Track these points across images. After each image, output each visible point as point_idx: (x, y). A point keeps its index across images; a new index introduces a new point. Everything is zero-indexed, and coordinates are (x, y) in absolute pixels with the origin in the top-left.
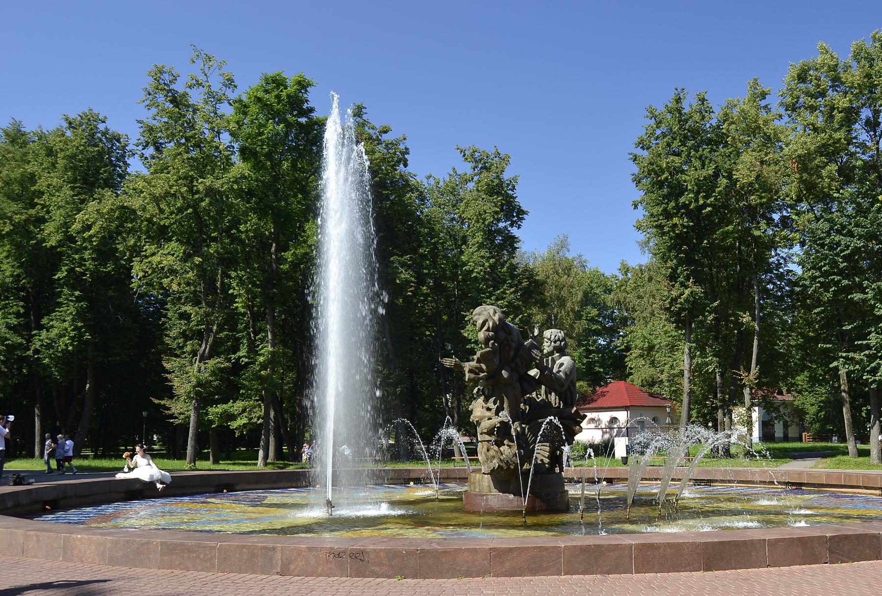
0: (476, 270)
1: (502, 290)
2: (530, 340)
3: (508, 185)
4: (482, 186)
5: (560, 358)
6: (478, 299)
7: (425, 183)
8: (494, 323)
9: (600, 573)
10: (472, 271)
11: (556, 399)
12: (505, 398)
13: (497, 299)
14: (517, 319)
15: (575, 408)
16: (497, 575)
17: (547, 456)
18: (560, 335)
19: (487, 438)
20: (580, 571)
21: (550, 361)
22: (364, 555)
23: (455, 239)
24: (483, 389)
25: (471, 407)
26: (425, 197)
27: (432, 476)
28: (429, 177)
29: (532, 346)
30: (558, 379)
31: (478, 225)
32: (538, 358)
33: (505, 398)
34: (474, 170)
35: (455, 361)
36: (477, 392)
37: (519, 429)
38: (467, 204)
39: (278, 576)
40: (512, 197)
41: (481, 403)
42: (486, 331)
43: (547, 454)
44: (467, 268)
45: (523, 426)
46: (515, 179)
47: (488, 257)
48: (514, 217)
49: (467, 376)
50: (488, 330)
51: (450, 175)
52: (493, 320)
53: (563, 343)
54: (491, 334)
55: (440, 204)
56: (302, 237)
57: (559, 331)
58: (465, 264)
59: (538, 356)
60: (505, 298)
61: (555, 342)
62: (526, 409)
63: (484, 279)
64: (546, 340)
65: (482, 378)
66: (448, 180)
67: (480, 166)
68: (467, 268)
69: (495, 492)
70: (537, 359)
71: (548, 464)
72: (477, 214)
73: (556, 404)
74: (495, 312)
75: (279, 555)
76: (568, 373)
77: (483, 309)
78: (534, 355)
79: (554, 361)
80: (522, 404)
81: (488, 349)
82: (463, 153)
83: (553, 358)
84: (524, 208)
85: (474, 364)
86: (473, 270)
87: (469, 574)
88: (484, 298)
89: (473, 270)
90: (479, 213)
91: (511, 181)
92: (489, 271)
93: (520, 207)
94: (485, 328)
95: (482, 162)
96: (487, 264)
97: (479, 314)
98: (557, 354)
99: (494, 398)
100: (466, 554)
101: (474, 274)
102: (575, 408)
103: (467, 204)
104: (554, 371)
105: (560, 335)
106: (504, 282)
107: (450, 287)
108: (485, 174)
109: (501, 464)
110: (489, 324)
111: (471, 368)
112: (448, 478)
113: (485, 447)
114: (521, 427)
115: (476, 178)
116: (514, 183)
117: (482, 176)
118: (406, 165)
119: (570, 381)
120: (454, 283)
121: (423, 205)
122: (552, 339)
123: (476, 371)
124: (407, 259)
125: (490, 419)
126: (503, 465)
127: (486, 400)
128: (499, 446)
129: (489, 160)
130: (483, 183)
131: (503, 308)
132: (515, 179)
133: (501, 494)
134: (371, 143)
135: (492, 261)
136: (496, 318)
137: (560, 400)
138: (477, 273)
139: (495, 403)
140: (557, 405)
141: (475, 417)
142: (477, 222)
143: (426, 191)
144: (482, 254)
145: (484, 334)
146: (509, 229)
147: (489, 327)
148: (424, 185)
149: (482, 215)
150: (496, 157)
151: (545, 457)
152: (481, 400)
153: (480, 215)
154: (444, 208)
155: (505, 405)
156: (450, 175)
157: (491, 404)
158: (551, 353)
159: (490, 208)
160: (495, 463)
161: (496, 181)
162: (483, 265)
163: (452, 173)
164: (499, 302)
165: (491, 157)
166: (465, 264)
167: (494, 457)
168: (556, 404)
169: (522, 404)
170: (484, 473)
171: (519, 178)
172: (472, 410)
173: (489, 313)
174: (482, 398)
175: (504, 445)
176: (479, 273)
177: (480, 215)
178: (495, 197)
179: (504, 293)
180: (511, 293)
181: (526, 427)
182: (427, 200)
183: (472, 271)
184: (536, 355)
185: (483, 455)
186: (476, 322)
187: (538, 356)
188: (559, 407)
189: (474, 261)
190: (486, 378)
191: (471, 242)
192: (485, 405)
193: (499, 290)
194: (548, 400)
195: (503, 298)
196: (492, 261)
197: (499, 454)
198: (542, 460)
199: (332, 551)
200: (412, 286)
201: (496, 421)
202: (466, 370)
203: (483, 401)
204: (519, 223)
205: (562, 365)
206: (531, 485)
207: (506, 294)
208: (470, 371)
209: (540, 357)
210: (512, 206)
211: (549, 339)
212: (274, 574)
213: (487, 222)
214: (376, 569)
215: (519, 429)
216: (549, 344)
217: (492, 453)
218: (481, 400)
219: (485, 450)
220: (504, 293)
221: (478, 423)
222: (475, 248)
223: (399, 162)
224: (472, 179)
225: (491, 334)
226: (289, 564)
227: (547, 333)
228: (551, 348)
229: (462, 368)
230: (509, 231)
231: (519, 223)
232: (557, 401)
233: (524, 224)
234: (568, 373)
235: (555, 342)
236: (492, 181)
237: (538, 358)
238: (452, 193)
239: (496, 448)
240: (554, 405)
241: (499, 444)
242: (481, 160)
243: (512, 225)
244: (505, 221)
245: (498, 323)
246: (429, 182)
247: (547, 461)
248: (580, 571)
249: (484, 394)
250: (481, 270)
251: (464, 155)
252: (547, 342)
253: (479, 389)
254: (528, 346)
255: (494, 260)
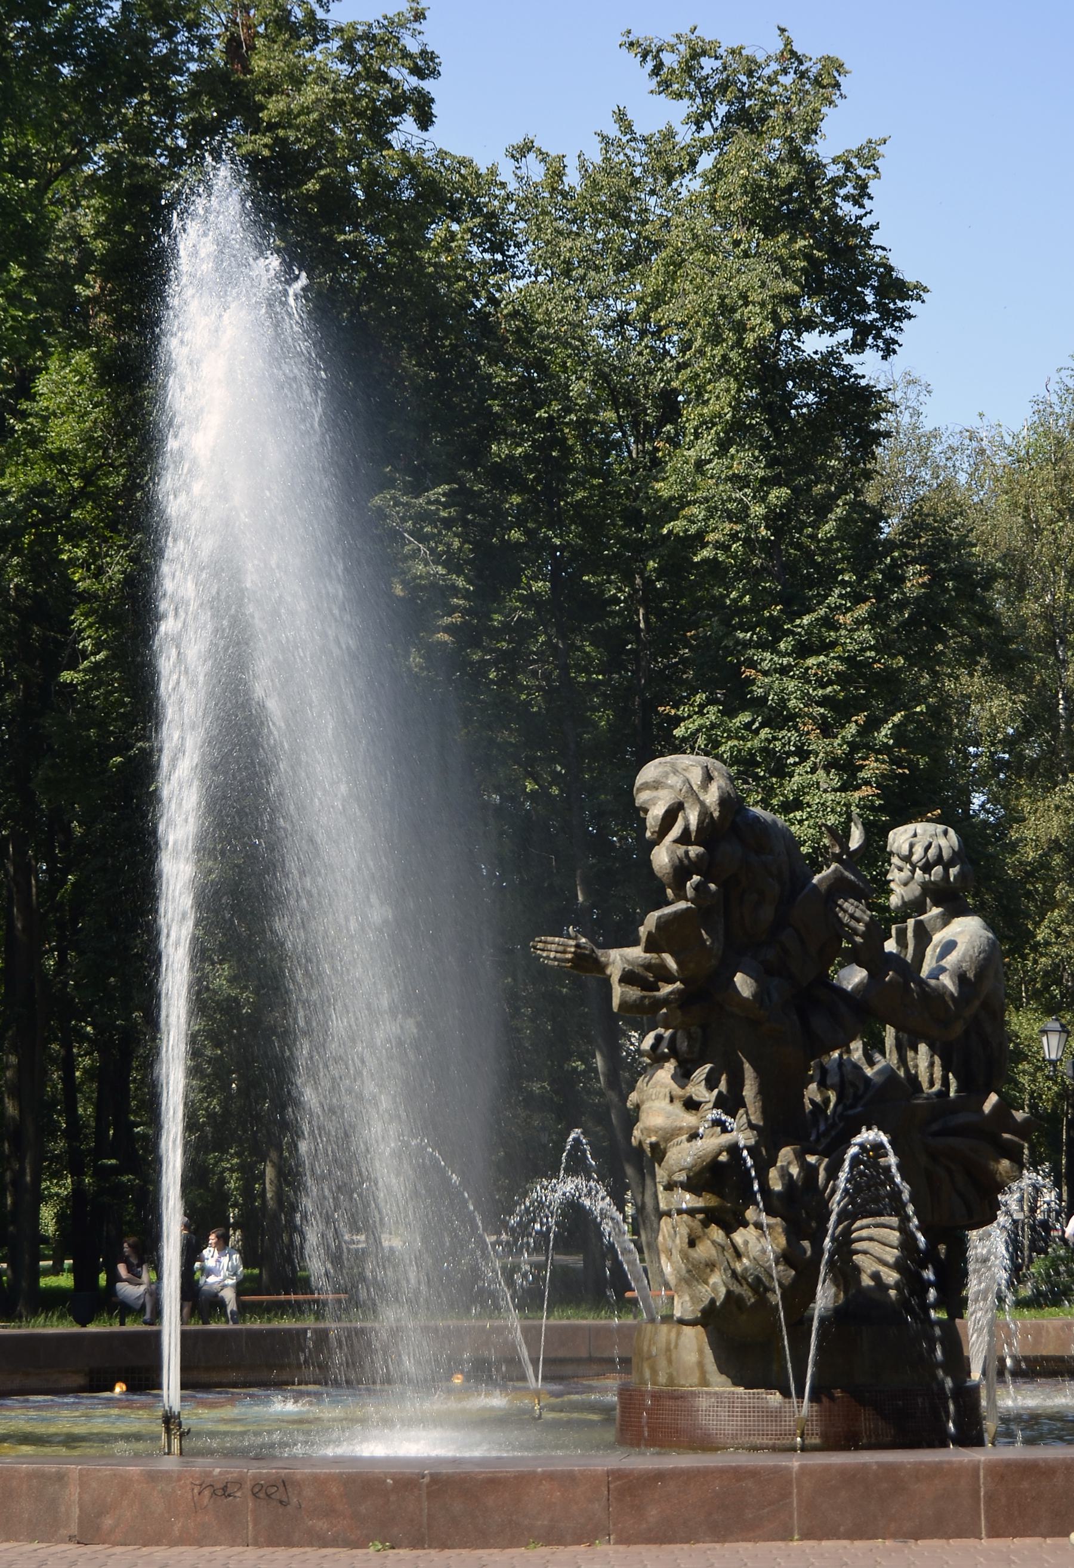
0: (711, 537)
1: (822, 611)
2: (833, 866)
3: (838, 182)
4: (729, 196)
5: (946, 923)
6: (729, 652)
7: (506, 173)
8: (705, 813)
9: (894, 1536)
10: (699, 540)
11: (932, 1065)
12: (747, 1065)
13: (803, 650)
14: (885, 730)
15: (993, 1098)
16: (625, 1540)
17: (891, 1260)
18: (943, 842)
19: (688, 1200)
20: (842, 1529)
21: (910, 934)
22: (290, 1489)
23: (631, 403)
24: (673, 1037)
25: (634, 1097)
26: (509, 234)
27: (524, 1353)
28: (525, 149)
29: (839, 888)
30: (932, 997)
31: (719, 351)
32: (861, 927)
33: (747, 1065)
34: (700, 128)
35: (577, 946)
36: (654, 1047)
37: (795, 1171)
38: (676, 264)
39: (72, 1546)
40: (855, 230)
41: (665, 1086)
42: (676, 841)
43: (891, 1255)
44: (677, 526)
45: (812, 1159)
46: (868, 155)
47: (763, 481)
48: (865, 308)
49: (618, 992)
50: (685, 838)
51: (605, 139)
52: (702, 804)
53: (953, 871)
54: (694, 851)
55: (568, 262)
56: (22, 416)
57: (941, 828)
58: (670, 509)
59: (858, 920)
60: (833, 644)
61: (927, 868)
62: (827, 1101)
63: (744, 569)
64: (895, 860)
65: (665, 1001)
66: (598, 159)
67: (722, 110)
68: (677, 526)
69: (720, 1384)
70: (855, 932)
71: (897, 1286)
72: (714, 305)
73: (932, 1084)
74: (708, 778)
75: (73, 1492)
76: (971, 975)
77: (668, 769)
78: (846, 919)
79: (923, 936)
80: (813, 1086)
81: (682, 905)
82: (650, 64)
83: (919, 925)
84: (906, 271)
85: (636, 953)
86: (700, 536)
87: (553, 1537)
88: (746, 644)
89: (700, 536)
90: (722, 305)
91: (848, 166)
92: (765, 540)
93: (890, 269)
94: (676, 831)
95: (729, 96)
96: (758, 510)
97: (656, 785)
98: (936, 911)
99: (708, 1066)
100: (546, 1486)
101: (706, 553)
102: (993, 1098)
103: (676, 264)
104: (924, 973)
105: (943, 842)
106: (828, 578)
107: (616, 600)
108: (742, 141)
109: (736, 1289)
110: (686, 820)
111: (628, 967)
112: (591, 1360)
113: (684, 1231)
114: (805, 1167)
115: (706, 162)
116: (862, 172)
117: (731, 149)
118: (425, 120)
119: (977, 1003)
120: (632, 585)
121: (500, 267)
122: (915, 858)
123: (646, 979)
124: (437, 502)
125: (694, 1136)
126: (745, 1292)
127: (683, 1076)
128: (729, 1230)
129: (760, 85)
130: (733, 182)
131: (823, 686)
132: (868, 155)
133: (741, 1389)
134: (287, 44)
135: (778, 494)
136: (711, 797)
137: (946, 1069)
138: (719, 546)
139: (711, 1083)
140: (937, 1087)
141: (648, 1131)
142: (715, 338)
143: (512, 207)
144: (738, 469)
145: (671, 853)
146: (848, 359)
147: (686, 830)
148: (503, 185)
149: (733, 310)
150: (785, 72)
151: (885, 1264)
152: (665, 1074)
153: (727, 310)
154: (583, 279)
155: (749, 1091)
156: (605, 139)
157: (698, 1090)
158: (916, 907)
159: (763, 285)
160: (717, 1285)
161: (788, 172)
162: (740, 515)
163: (613, 131)
164: (811, 661)
165: (767, 72)
166: (670, 509)
167: (711, 1266)
168: (932, 1084)
169: (813, 1086)
170: (682, 1322)
171: (881, 149)
172: (638, 1107)
173: (687, 781)
174: (670, 1066)
175: (745, 1224)
176: (725, 548)
177: (727, 310)
178: (784, 237)
179: (829, 623)
180: (859, 623)
181: (820, 1162)
182: (518, 245)
183: (699, 540)
184: (852, 916)
185: (677, 1256)
186: (646, 811)
187: (858, 920)
188: (943, 1094)
189: (707, 500)
190: (682, 1001)
191: (691, 416)
192: (677, 1091)
193: (813, 610)
194: (907, 1071)
195: (825, 647)
196: (778, 494)
197: (729, 1254)
198: (876, 1276)
199: (208, 1481)
200: (455, 609)
201: (711, 1143)
202: (615, 972)
203: (673, 1077)
204: (888, 333)
205: (949, 946)
206: (781, 1331)
207: (835, 626)
208: (628, 978)
209: (867, 925)
210: (856, 264)
211: (907, 859)
212: (62, 1541)
213: (750, 339)
214: (321, 1525)
215: (795, 1171)
216: (906, 874)
217: (704, 1251)
218: (665, 1074)
219: (680, 1241)
220: (829, 623)
221: (658, 1152)
222: (705, 446)
223: (397, 105)
224: (693, 163)
225: (694, 851)
226: (100, 1514)
227: (899, 838)
228: (914, 890)
229: (600, 967)
230: (848, 368)
231: (888, 333)
232: (938, 1072)
233: (908, 334)
234: (971, 975)
235: (927, 868)
236: (771, 172)
237: (861, 927)
238: (614, 215)
239: (716, 1233)
240: (925, 1085)
241: (731, 1221)
242: (723, 87)
243: (858, 346)
244: (832, 329)
245: (716, 814)
246: (522, 172)
247: (891, 1277)
248: (842, 1529)
249: (674, 1053)
250: (734, 536)
251: (657, 71)
252: (900, 869)
253: (659, 1039)
254: (823, 888)
255: (785, 492)
